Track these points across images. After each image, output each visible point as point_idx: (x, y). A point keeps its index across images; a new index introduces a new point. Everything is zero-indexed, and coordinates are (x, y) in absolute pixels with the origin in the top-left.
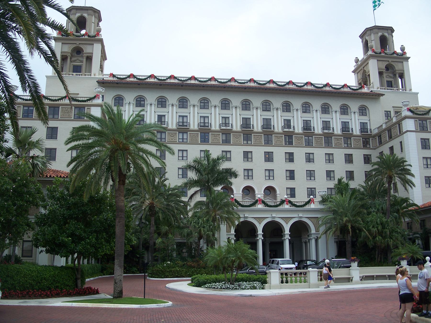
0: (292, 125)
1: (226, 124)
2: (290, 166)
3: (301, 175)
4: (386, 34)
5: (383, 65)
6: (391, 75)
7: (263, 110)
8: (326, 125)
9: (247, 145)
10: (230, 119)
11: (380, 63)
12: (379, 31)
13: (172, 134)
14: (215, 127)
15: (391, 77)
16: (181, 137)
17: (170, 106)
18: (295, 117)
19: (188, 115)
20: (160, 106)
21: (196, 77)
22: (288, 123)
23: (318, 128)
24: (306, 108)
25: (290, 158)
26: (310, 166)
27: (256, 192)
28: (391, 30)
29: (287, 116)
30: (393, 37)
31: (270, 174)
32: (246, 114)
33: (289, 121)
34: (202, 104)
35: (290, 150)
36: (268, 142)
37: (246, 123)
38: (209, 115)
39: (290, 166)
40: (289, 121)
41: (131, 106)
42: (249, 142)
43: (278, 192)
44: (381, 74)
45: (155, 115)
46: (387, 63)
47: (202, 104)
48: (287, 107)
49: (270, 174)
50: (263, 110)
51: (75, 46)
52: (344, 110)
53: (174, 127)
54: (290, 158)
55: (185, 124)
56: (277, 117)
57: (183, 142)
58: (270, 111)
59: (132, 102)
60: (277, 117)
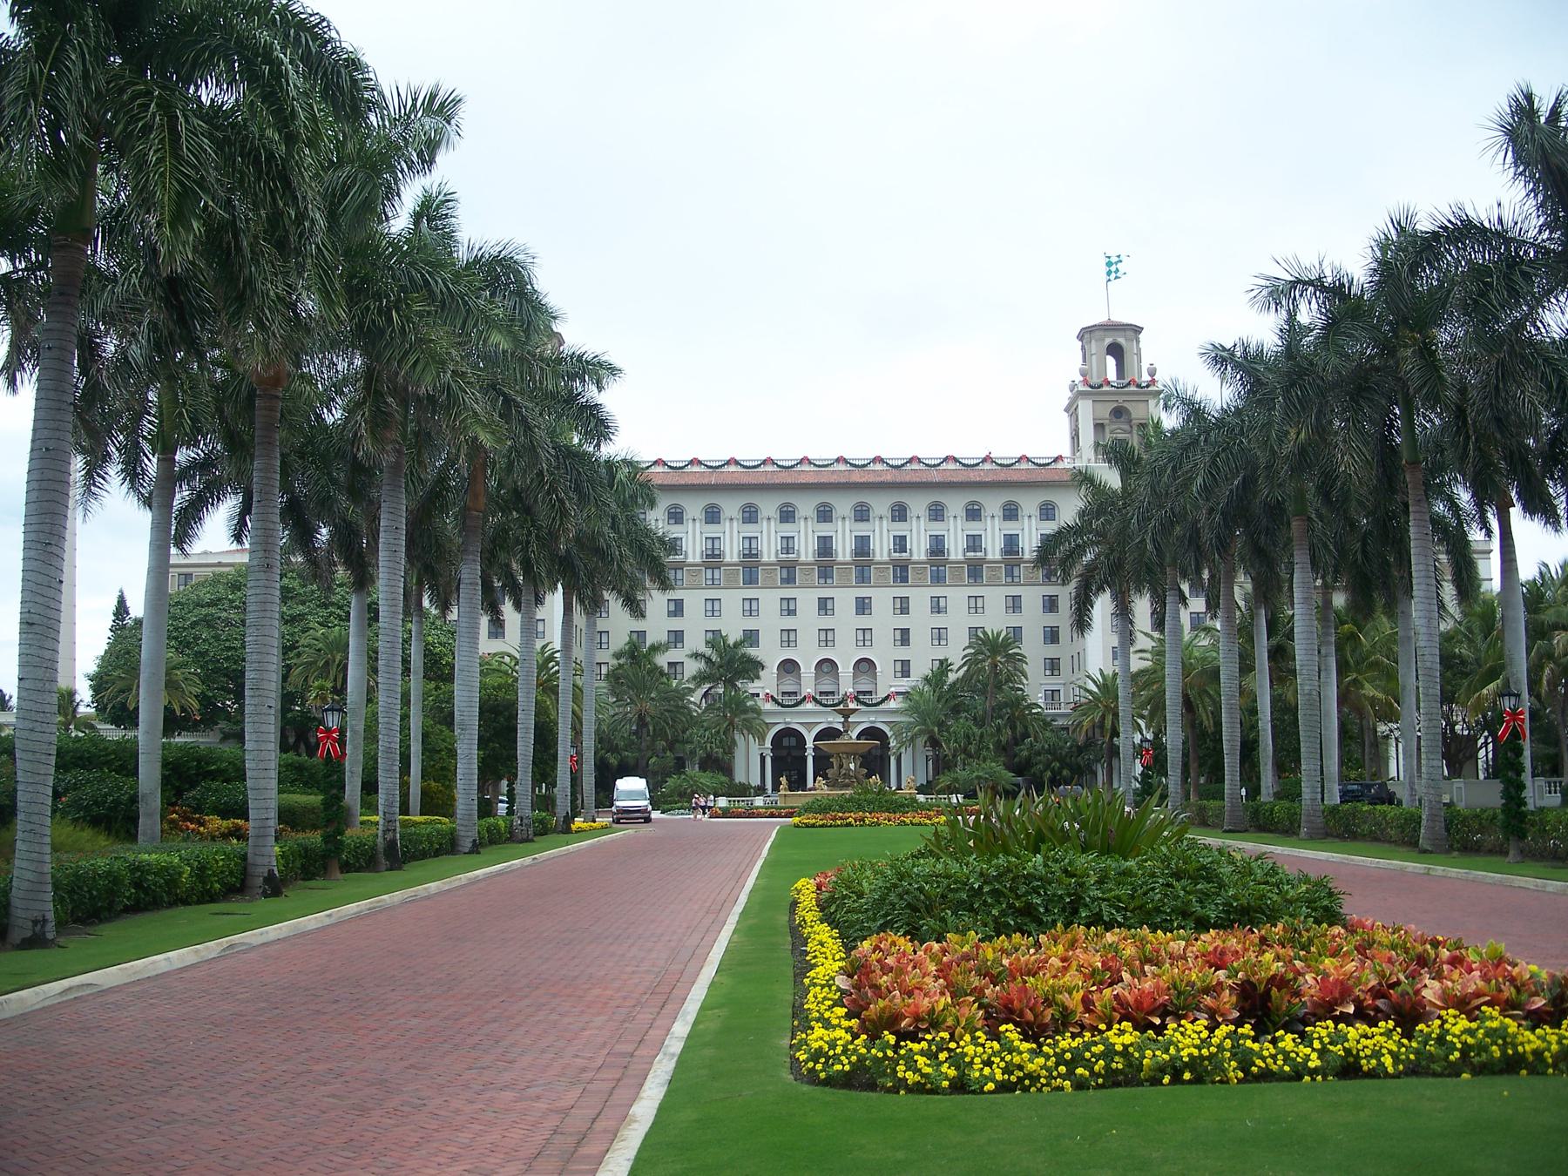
0: (908, 547)
1: (788, 549)
2: (903, 621)
3: (920, 637)
4: (1121, 340)
5: (1105, 411)
6: (1126, 427)
7: (856, 520)
8: (974, 543)
9: (1013, 583)
10: (796, 539)
11: (1099, 405)
12: (1107, 333)
13: (694, 571)
14: (882, 555)
15: (1125, 432)
16: (709, 576)
17: (877, 519)
18: (952, 531)
19: (721, 535)
20: (672, 521)
21: (737, 458)
22: (901, 543)
23: (956, 549)
24: (937, 513)
25: (903, 606)
26: (939, 621)
27: (802, 670)
28: (1137, 330)
29: (900, 529)
30: (1138, 342)
31: (865, 635)
33: (904, 538)
34: (747, 515)
35: (902, 592)
37: (825, 546)
38: (759, 535)
39: (903, 621)
40: (904, 538)
41: (698, 524)
42: (829, 581)
43: (878, 669)
44: (1099, 427)
45: (813, 537)
46: (1115, 405)
47: (747, 515)
48: (900, 513)
49: (865, 635)
50: (856, 520)
52: (937, 513)
53: (698, 560)
54: (903, 606)
56: (919, 533)
57: (714, 585)
58: (868, 520)
60: (919, 533)
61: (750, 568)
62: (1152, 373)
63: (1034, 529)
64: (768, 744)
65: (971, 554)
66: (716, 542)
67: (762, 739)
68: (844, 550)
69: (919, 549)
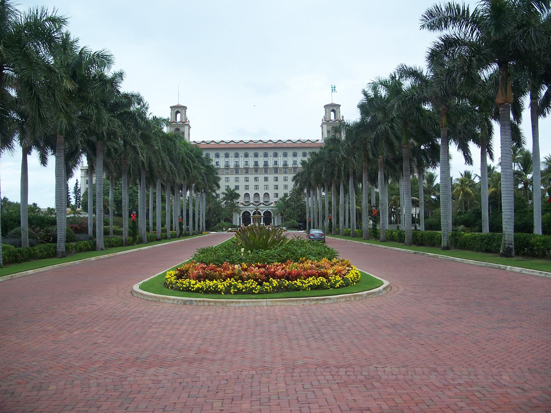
31: (256, 187)
32: (285, 159)
33: (277, 161)
36: (266, 172)
51: (176, 128)
52: (285, 155)
55: (228, 165)
59: (233, 156)
61: (256, 169)
62: (343, 117)
63: (223, 160)
64: (241, 215)
65: (294, 166)
66: (228, 163)
67: (240, 214)
68: (261, 165)
69: (261, 165)
